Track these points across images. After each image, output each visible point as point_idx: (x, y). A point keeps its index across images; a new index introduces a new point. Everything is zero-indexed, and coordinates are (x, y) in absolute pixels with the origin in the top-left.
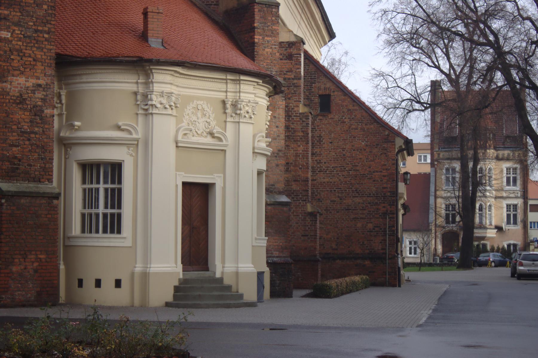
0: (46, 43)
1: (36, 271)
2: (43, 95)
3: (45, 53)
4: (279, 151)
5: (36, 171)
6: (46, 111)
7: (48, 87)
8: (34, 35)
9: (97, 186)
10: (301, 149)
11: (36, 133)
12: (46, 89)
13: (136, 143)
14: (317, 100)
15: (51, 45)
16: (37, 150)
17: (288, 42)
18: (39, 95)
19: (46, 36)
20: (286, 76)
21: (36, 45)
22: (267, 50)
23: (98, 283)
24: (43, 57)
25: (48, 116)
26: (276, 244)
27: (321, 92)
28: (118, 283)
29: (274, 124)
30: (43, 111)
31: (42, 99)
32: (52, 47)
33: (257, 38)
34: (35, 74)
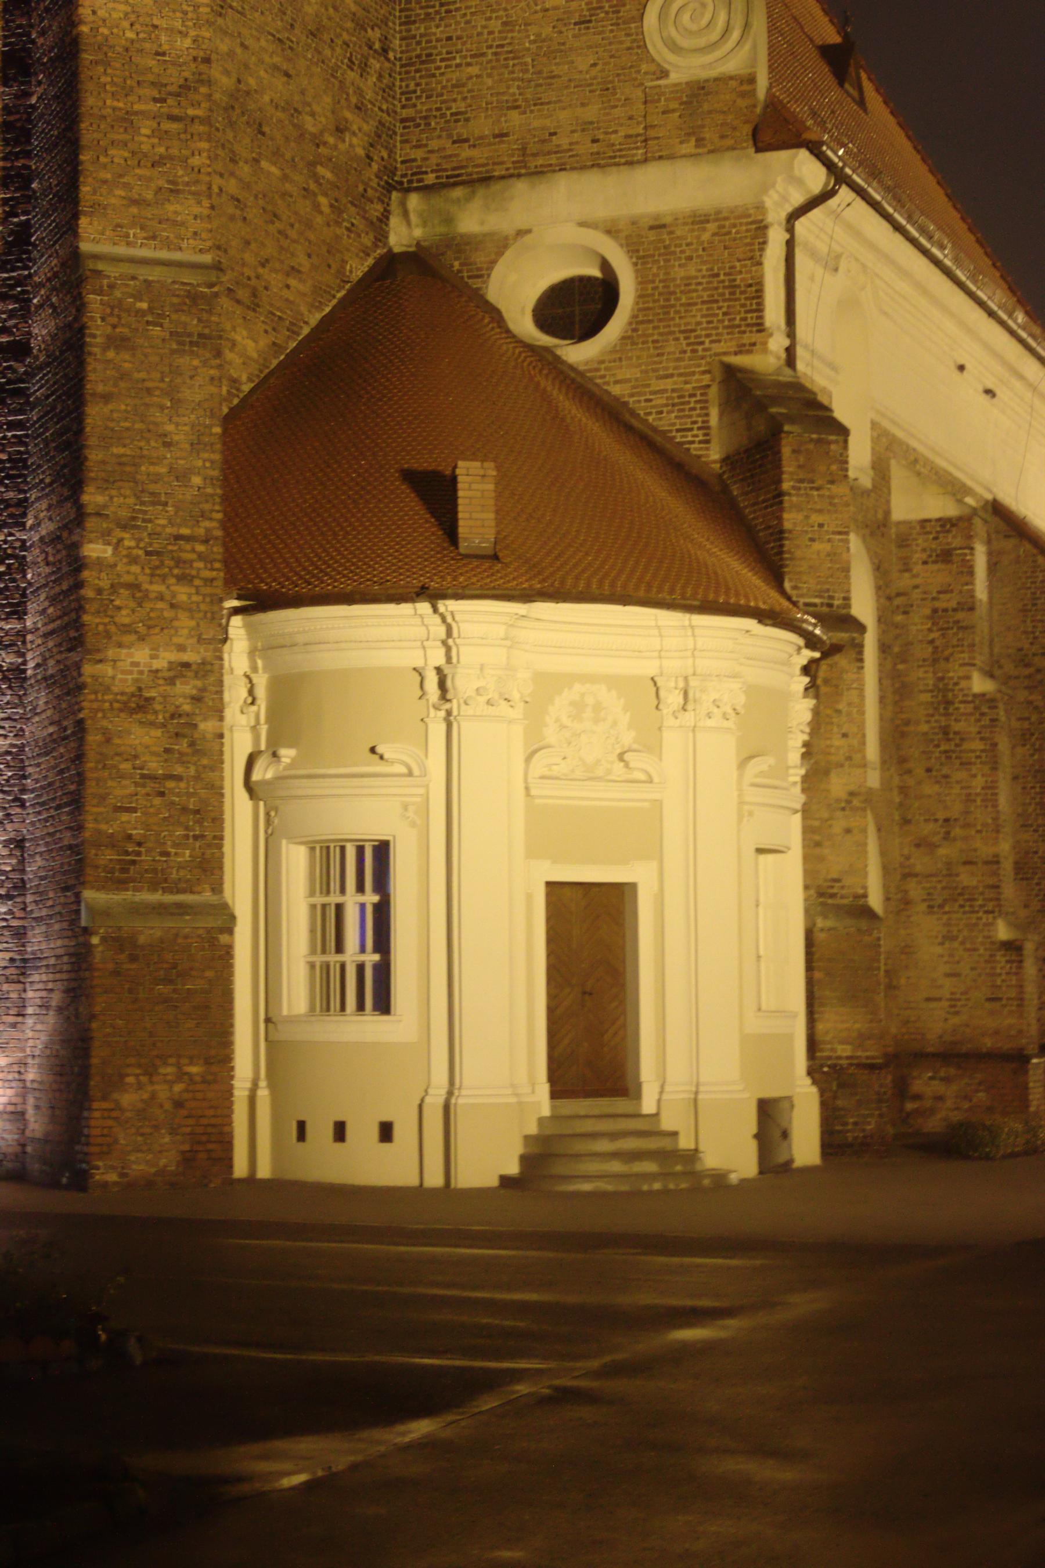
0: (201, 565)
1: (179, 1104)
2: (195, 687)
3: (197, 587)
4: (852, 794)
5: (181, 867)
6: (202, 726)
7: (208, 667)
8: (170, 548)
9: (339, 899)
11: (179, 778)
12: (201, 673)
13: (422, 791)
15: (212, 569)
16: (182, 819)
17: (939, 520)
18: (185, 688)
19: (201, 548)
20: (937, 604)
21: (176, 571)
22: (817, 546)
23: (340, 1132)
24: (195, 598)
25: (209, 736)
26: (845, 1026)
28: (386, 1132)
29: (835, 730)
30: (195, 726)
31: (193, 698)
32: (214, 573)
33: (790, 519)
34: (175, 640)
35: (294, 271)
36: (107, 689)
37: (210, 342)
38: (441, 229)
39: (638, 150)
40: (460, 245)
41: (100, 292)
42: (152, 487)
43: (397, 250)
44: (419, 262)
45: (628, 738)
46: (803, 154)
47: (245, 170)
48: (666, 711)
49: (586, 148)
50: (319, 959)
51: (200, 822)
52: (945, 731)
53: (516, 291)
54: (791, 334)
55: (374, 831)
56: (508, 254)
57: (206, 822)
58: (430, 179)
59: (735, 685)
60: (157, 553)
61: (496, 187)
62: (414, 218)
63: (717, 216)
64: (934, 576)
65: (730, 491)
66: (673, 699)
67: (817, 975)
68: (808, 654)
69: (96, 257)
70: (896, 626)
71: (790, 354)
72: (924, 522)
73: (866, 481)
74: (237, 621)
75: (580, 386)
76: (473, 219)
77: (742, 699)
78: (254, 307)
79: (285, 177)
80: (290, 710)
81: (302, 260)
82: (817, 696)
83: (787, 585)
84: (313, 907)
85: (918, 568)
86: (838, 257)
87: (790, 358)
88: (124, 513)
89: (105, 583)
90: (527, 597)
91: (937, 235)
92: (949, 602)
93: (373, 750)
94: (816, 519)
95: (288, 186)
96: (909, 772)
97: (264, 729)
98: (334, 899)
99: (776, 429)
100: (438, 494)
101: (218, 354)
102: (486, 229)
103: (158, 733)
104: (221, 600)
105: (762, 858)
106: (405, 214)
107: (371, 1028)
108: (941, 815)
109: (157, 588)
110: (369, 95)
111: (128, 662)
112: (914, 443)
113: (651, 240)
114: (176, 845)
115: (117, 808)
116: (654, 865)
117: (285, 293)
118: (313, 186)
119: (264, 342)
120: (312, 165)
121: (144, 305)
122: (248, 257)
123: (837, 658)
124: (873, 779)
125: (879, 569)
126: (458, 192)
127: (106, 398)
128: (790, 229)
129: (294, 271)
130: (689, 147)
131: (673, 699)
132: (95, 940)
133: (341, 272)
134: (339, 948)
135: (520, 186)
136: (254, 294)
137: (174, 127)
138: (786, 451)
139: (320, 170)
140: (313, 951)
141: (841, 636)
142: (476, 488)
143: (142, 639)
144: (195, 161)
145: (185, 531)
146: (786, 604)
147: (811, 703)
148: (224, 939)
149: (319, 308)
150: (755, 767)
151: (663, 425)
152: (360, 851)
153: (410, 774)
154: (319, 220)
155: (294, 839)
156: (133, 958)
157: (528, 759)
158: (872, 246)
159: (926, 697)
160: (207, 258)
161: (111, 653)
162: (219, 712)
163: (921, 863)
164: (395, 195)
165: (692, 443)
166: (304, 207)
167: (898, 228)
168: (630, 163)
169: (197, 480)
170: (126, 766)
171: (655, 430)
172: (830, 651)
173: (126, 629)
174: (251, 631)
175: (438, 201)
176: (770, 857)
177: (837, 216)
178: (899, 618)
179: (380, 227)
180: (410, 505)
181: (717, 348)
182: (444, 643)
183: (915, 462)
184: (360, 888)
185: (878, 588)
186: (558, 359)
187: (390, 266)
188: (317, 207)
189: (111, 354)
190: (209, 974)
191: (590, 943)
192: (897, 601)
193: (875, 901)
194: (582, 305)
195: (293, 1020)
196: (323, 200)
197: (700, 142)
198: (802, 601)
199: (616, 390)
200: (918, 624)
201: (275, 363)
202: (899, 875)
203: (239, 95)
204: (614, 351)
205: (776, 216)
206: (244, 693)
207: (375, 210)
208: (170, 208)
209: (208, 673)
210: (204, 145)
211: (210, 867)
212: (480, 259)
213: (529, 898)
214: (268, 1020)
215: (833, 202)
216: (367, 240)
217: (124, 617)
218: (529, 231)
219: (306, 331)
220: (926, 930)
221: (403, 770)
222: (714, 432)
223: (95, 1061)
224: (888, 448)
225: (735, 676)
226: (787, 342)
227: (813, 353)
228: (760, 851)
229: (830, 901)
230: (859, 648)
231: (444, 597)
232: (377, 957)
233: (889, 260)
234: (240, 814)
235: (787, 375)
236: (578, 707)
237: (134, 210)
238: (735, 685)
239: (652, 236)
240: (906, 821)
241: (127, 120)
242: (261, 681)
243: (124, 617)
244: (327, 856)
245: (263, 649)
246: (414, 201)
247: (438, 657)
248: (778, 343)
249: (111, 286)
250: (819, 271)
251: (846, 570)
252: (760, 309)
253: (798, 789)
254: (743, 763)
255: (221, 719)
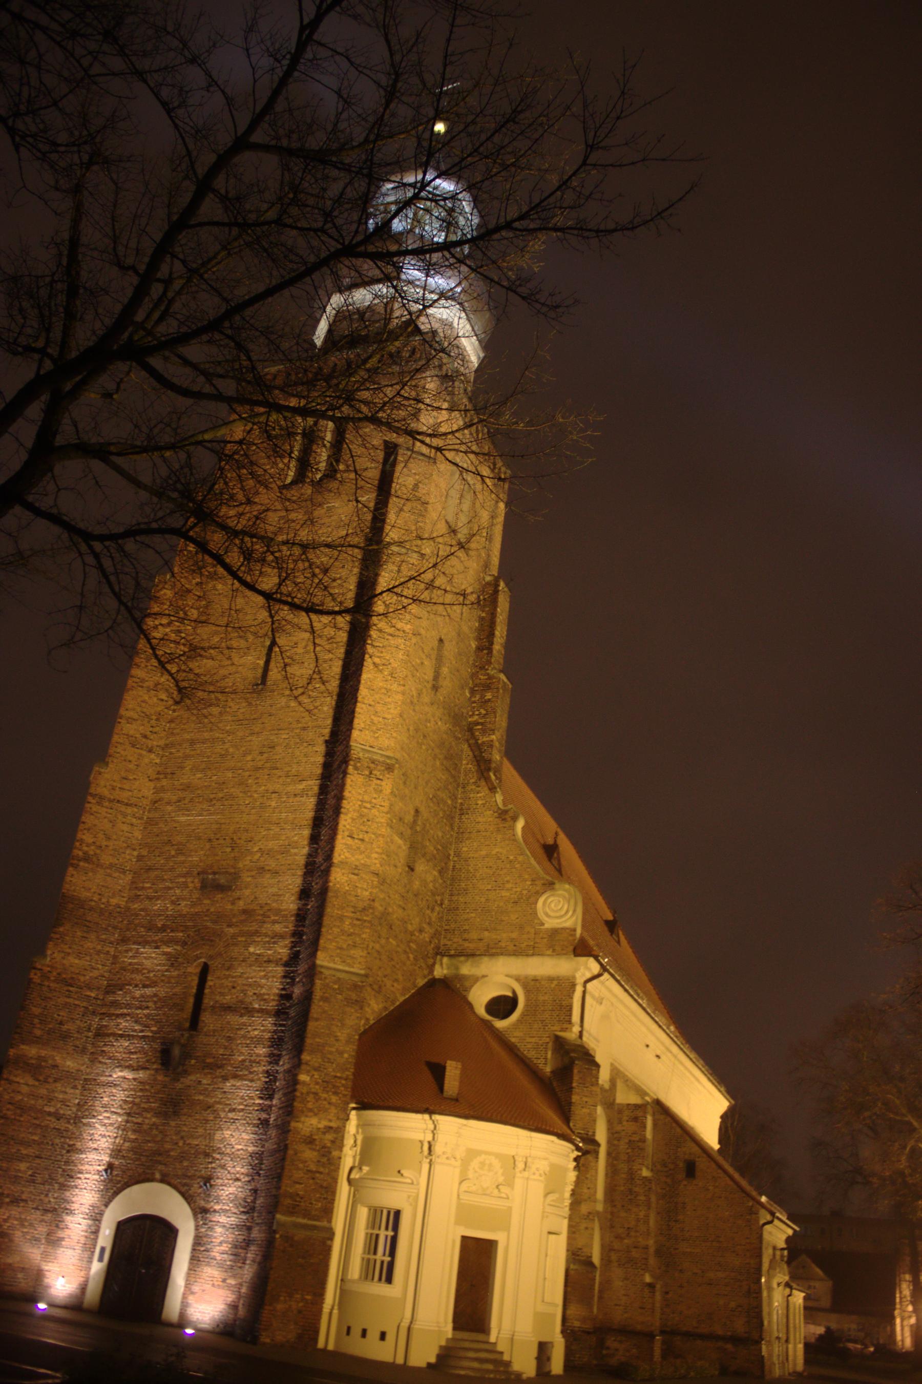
4: (590, 1213)
5: (316, 1210)
10: (642, 1214)
14: (681, 1165)
18: (329, 1137)
19: (343, 1082)
22: (584, 1110)
27: (687, 1157)
33: (575, 1098)
35: (396, 980)
36: (299, 1133)
37: (360, 1004)
38: (454, 972)
39: (532, 951)
40: (461, 978)
41: (321, 979)
42: (329, 1056)
43: (437, 977)
44: (445, 984)
45: (501, 1179)
46: (592, 959)
47: (383, 941)
48: (517, 1170)
49: (511, 948)
50: (367, 1256)
51: (327, 1192)
52: (630, 1191)
53: (480, 998)
54: (582, 1026)
55: (395, 1204)
56: (478, 984)
57: (330, 1191)
58: (452, 952)
59: (546, 1163)
60: (327, 1082)
61: (477, 958)
62: (444, 966)
63: (558, 979)
64: (630, 1127)
65: (547, 1084)
66: (520, 1165)
67: (569, 1289)
68: (576, 1153)
69: (322, 967)
70: (614, 1145)
71: (581, 1033)
72: (629, 1105)
73: (607, 1086)
74: (353, 1113)
75: (499, 1036)
76: (466, 969)
77: (548, 1169)
78: (379, 992)
79: (398, 946)
80: (370, 1150)
81: (400, 977)
82: (579, 1171)
83: (571, 1124)
84: (367, 1234)
85: (625, 1123)
86: (602, 999)
87: (581, 1036)
88: (316, 1065)
89: (305, 1090)
90: (467, 1117)
91: (641, 995)
92: (636, 1138)
93: (399, 1172)
94: (585, 1099)
95: (399, 949)
96: (615, 1206)
97: (358, 1158)
98: (376, 1232)
99: (574, 1060)
100: (438, 1072)
101: (361, 1008)
102: (471, 973)
103: (315, 1153)
104: (348, 1104)
105: (551, 1236)
106: (441, 964)
107: (382, 1289)
108: (626, 1226)
109: (325, 1095)
110: (433, 919)
111: (309, 1124)
112: (627, 1073)
113: (532, 985)
114: (316, 1200)
115: (296, 1183)
116: (506, 1234)
117: (392, 989)
118: (408, 950)
119: (381, 1006)
120: (409, 942)
121: (336, 987)
122: (380, 973)
123: (588, 1156)
124: (600, 1207)
125: (610, 1122)
126: (462, 959)
127: (317, 1020)
128: (585, 987)
129: (396, 980)
130: (549, 952)
131: (520, 1165)
132: (277, 1236)
133: (414, 983)
134: (375, 1253)
135: (486, 959)
136: (380, 987)
137: (358, 922)
138: (575, 1071)
139: (411, 944)
140: (364, 1253)
141: (591, 1147)
142: (453, 1072)
143: (316, 1115)
144: (364, 936)
145: (339, 1075)
146: (569, 1131)
147: (576, 1173)
148: (329, 1242)
149: (404, 995)
150: (551, 1197)
151: (529, 1056)
152: (389, 1213)
153: (412, 1183)
154: (408, 963)
155: (364, 1205)
156: (291, 1246)
157: (460, 1183)
158: (616, 996)
159: (624, 1176)
160: (363, 972)
161: (303, 1119)
162: (341, 1148)
163: (617, 1245)
164: (439, 957)
165: (540, 1063)
166: (403, 957)
167: (626, 990)
168: (527, 955)
169: (346, 1055)
170: (301, 1165)
171: (526, 1057)
172: (585, 1153)
173: (311, 1110)
174: (359, 1117)
175: (454, 961)
176: (554, 1236)
177: (603, 983)
178: (616, 1142)
179: (431, 968)
180: (427, 1076)
181: (555, 1028)
182: (433, 1132)
183: (627, 1081)
184: (387, 1228)
185: (608, 1129)
186: (492, 1026)
187: (433, 983)
188: (408, 958)
189: (321, 1003)
190: (321, 1257)
191: (477, 1263)
192: (616, 1135)
193: (596, 1260)
194: (503, 1006)
195: (353, 1281)
196: (411, 956)
197: (554, 951)
198: (576, 1131)
199: (513, 1040)
200: (623, 1146)
201: (384, 1014)
202: (607, 1250)
203: (385, 914)
204: (514, 1025)
205: (580, 980)
206: (352, 1142)
207: (431, 961)
208: (352, 952)
209: (339, 1132)
210: (368, 930)
211: (328, 1211)
212: (467, 984)
213: (454, 1241)
214: (342, 1280)
215: (602, 978)
216: (426, 972)
217: (310, 1105)
218: (486, 976)
219: (398, 1003)
220: (617, 1273)
221: (410, 1181)
222: (549, 1061)
223: (269, 1288)
224: (617, 1074)
225: (546, 1159)
226: (580, 1029)
227: (590, 1034)
228: (550, 1233)
229: (577, 1259)
230: (597, 1153)
231: (435, 1113)
232: (389, 1259)
233: (622, 1002)
234: (344, 1191)
235: (579, 1042)
236: (483, 1164)
237: (338, 951)
238: (546, 1163)
239: (532, 983)
240: (612, 1227)
241: (341, 918)
242: (360, 1138)
243: (310, 1105)
244: (375, 1212)
245: (362, 1125)
246: (445, 960)
247: (429, 1137)
248: (576, 1029)
249: (325, 978)
250: (595, 1003)
251: (595, 1121)
252: (570, 1015)
253: (567, 1209)
254: (546, 1195)
255: (341, 1151)
